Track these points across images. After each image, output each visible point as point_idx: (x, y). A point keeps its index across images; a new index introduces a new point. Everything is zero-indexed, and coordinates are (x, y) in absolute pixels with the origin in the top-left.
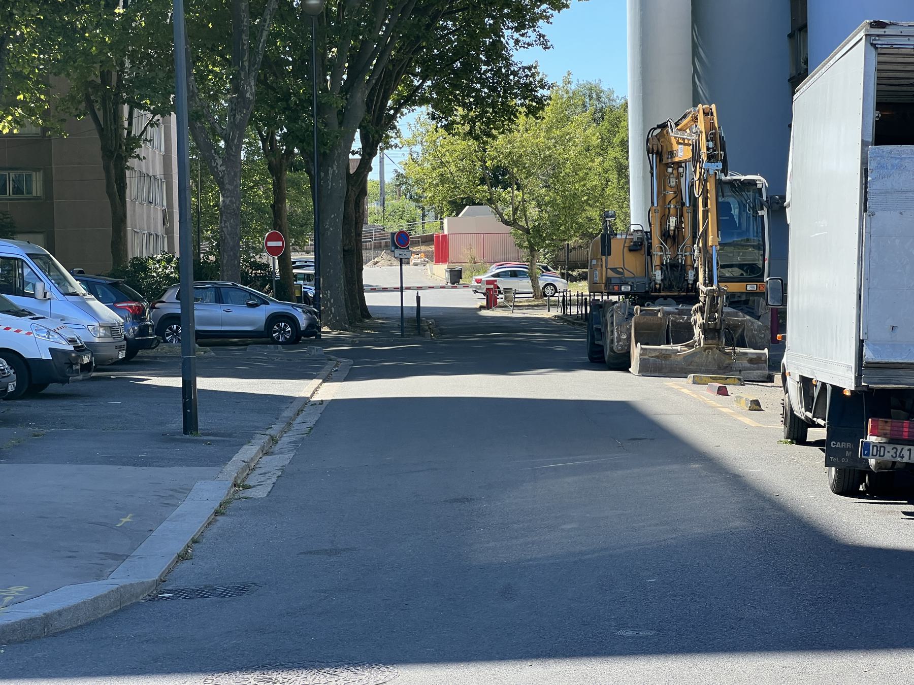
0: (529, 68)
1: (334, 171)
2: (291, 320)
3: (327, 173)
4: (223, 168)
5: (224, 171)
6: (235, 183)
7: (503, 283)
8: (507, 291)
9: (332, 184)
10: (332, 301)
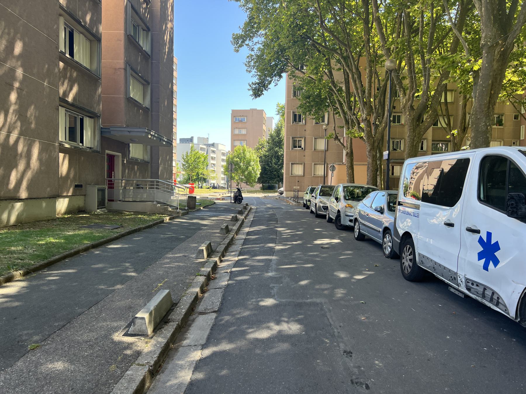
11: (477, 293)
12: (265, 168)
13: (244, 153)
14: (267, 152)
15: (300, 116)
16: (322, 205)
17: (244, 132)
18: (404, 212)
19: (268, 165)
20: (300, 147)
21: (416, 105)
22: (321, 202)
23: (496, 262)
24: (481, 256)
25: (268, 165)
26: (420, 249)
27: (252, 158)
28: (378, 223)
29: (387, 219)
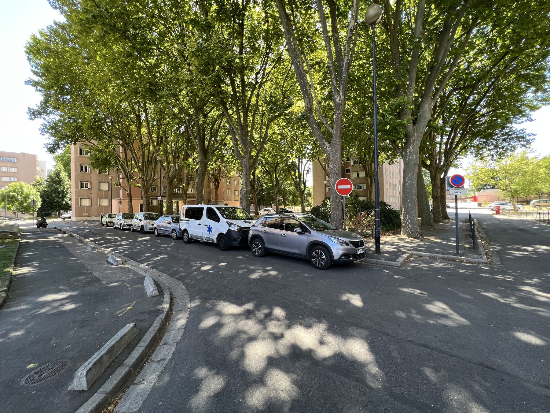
0: (523, 130)
1: (411, 150)
2: (326, 249)
3: (406, 152)
4: (330, 149)
5: (330, 150)
6: (336, 156)
7: (501, 207)
8: (503, 209)
9: (409, 157)
10: (409, 221)
11: (208, 240)
12: (45, 200)
13: (21, 188)
14: (46, 188)
15: (86, 168)
16: (126, 224)
17: (13, 170)
18: (183, 223)
19: (48, 198)
20: (87, 187)
21: (170, 176)
22: (125, 222)
23: (211, 231)
24: (208, 231)
25: (48, 198)
26: (190, 233)
27: (31, 192)
28: (170, 228)
29: (173, 226)
